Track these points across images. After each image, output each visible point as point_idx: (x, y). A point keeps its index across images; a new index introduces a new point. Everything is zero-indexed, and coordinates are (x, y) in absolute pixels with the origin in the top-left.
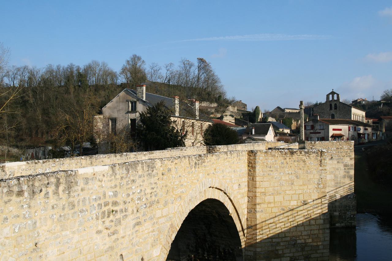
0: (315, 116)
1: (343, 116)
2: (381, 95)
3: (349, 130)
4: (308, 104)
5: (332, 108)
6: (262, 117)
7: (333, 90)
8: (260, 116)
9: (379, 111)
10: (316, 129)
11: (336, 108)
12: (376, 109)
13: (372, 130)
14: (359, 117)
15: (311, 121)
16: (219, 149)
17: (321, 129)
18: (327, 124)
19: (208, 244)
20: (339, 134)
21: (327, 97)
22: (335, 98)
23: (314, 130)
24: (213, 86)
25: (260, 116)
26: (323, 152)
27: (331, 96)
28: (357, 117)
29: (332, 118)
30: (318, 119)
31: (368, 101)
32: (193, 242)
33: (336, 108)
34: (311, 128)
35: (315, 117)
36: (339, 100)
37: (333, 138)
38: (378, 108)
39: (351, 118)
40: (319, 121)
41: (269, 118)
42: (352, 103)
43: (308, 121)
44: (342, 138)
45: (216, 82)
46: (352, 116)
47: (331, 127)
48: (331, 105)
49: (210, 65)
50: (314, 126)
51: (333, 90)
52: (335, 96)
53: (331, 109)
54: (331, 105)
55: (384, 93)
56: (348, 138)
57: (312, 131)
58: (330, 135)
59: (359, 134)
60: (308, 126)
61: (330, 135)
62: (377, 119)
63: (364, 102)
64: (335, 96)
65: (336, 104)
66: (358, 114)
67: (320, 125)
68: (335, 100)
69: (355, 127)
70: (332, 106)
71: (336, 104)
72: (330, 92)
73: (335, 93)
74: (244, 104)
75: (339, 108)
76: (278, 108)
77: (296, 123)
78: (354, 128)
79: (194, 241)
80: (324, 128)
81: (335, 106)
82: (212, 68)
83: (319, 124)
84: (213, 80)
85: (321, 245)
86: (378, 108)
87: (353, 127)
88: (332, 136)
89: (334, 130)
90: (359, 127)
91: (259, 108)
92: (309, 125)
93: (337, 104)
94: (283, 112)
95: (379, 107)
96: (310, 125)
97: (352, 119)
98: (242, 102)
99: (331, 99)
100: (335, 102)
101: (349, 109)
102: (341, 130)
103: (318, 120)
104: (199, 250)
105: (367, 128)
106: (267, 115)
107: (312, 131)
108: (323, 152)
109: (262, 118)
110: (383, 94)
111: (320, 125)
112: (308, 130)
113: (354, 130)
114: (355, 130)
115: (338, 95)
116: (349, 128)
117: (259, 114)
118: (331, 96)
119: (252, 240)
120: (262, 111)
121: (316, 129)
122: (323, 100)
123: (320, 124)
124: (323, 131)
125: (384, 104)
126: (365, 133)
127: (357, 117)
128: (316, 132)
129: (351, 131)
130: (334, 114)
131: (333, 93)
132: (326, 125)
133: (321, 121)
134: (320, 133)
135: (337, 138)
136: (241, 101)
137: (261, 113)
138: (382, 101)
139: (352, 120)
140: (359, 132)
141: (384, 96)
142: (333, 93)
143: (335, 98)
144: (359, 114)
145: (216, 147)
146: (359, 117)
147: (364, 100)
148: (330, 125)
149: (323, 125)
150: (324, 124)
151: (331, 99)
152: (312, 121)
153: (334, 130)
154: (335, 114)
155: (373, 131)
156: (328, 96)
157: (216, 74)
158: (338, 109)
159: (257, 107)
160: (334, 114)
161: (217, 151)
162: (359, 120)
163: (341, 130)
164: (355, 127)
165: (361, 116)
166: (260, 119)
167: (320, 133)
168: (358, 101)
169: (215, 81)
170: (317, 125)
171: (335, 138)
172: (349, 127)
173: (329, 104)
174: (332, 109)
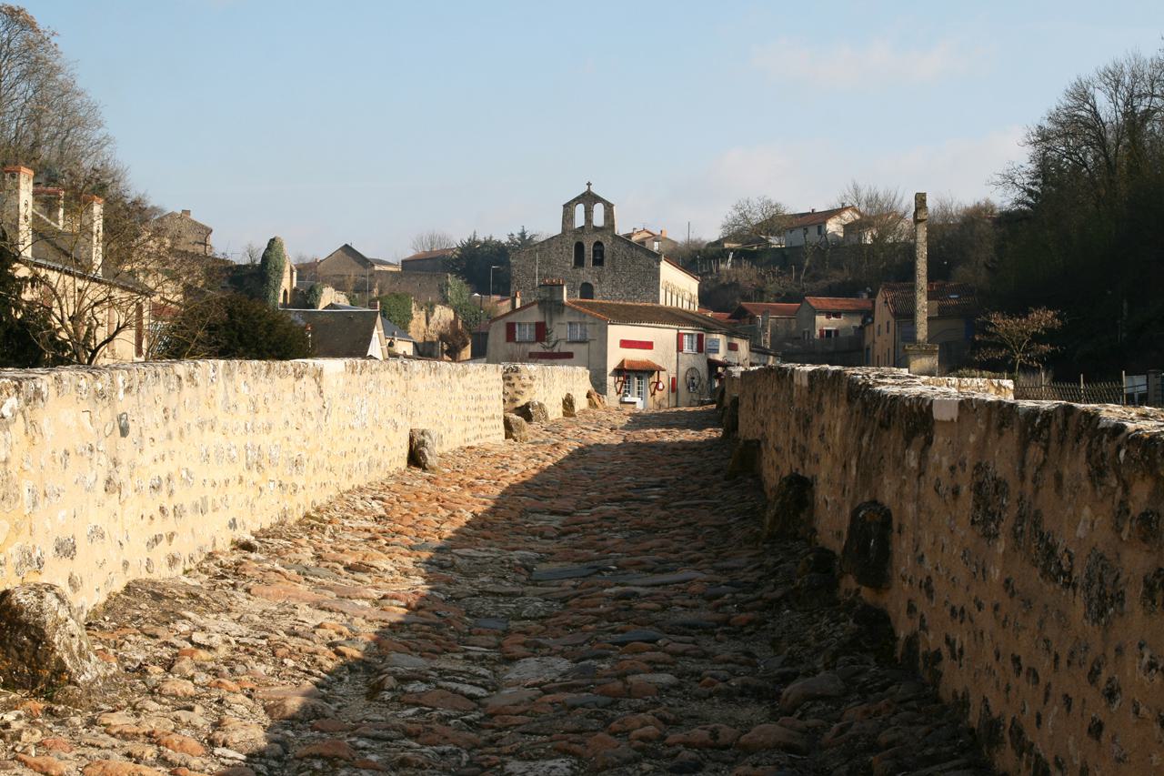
0: (554, 285)
1: (628, 293)
2: (725, 220)
3: (680, 348)
4: (432, 243)
5: (586, 258)
6: (295, 285)
7: (589, 184)
8: (287, 283)
9: (724, 280)
10: (554, 339)
11: (598, 261)
12: (711, 272)
13: (751, 350)
14: (680, 300)
16: (530, 378)
17: (574, 338)
18: (599, 318)
20: (643, 363)
22: (598, 220)
23: (546, 344)
24: (69, 139)
25: (287, 283)
26: (1004, 388)
28: (674, 297)
29: (581, 297)
30: (565, 299)
31: (675, 243)
33: (598, 261)
34: (534, 333)
35: (551, 290)
36: (613, 226)
37: (621, 379)
38: (717, 271)
39: (658, 302)
40: (570, 307)
41: (325, 290)
44: (651, 380)
45: (81, 123)
46: (662, 292)
47: (616, 332)
48: (579, 247)
49: (54, 40)
50: (548, 326)
51: (589, 184)
52: (599, 210)
53: (579, 262)
54: (579, 247)
55: (736, 214)
56: (673, 379)
57: (537, 348)
58: (612, 364)
59: (713, 365)
60: (519, 324)
61: (612, 364)
62: (729, 314)
63: (656, 244)
64: (599, 210)
65: (598, 244)
66: (679, 286)
67: (570, 323)
68: (597, 229)
69: (700, 337)
70: (586, 250)
71: (598, 244)
73: (597, 199)
74: (203, 227)
75: (614, 259)
76: (347, 249)
77: (424, 317)
78: (695, 339)
80: (589, 337)
81: (594, 251)
82: (63, 56)
83: (566, 318)
84: (65, 111)
86: (717, 271)
87: (692, 334)
88: (619, 371)
89: (626, 344)
90: (715, 336)
91: (281, 244)
92: (525, 324)
93: (605, 245)
94: (366, 267)
95: (722, 266)
96: (530, 324)
97: (662, 302)
98: (193, 216)
99: (579, 220)
100: (599, 237)
101: (650, 266)
102: (648, 345)
103: (563, 305)
105: (736, 341)
106: (311, 276)
107: (537, 348)
108: (1003, 390)
109: (295, 291)
110: (729, 216)
111: (570, 323)
112: (520, 342)
113: (695, 346)
114: (700, 349)
115: (609, 207)
116: (680, 337)
117: (280, 272)
119: (571, 739)
120: (292, 254)
121: (554, 339)
122: (547, 225)
123: (571, 320)
124: (583, 348)
125: (740, 255)
126: (730, 359)
127: (674, 297)
128: (556, 350)
129: (686, 349)
130: (590, 285)
131: (589, 199)
132: (594, 324)
133: (574, 309)
135: (636, 379)
136: (187, 212)
137: (287, 269)
138: (726, 245)
139: (662, 307)
140: (712, 356)
141: (733, 226)
142: (589, 199)
143: (598, 220)
144: (670, 282)
145: (517, 370)
146: (680, 300)
147: (655, 238)
149: (581, 324)
150: (588, 319)
151: (579, 220)
152: (539, 307)
153: (626, 344)
154: (594, 285)
155: (755, 354)
156: (568, 208)
157: (80, 84)
158: (606, 263)
159: (273, 240)
160: (590, 282)
161: (523, 386)
162: (680, 306)
163: (648, 345)
164: (700, 337)
165: (687, 296)
166: (285, 292)
168: (634, 239)
169: (74, 120)
170: (559, 324)
171: (628, 377)
172: (678, 334)
173: (572, 242)
174: (586, 262)
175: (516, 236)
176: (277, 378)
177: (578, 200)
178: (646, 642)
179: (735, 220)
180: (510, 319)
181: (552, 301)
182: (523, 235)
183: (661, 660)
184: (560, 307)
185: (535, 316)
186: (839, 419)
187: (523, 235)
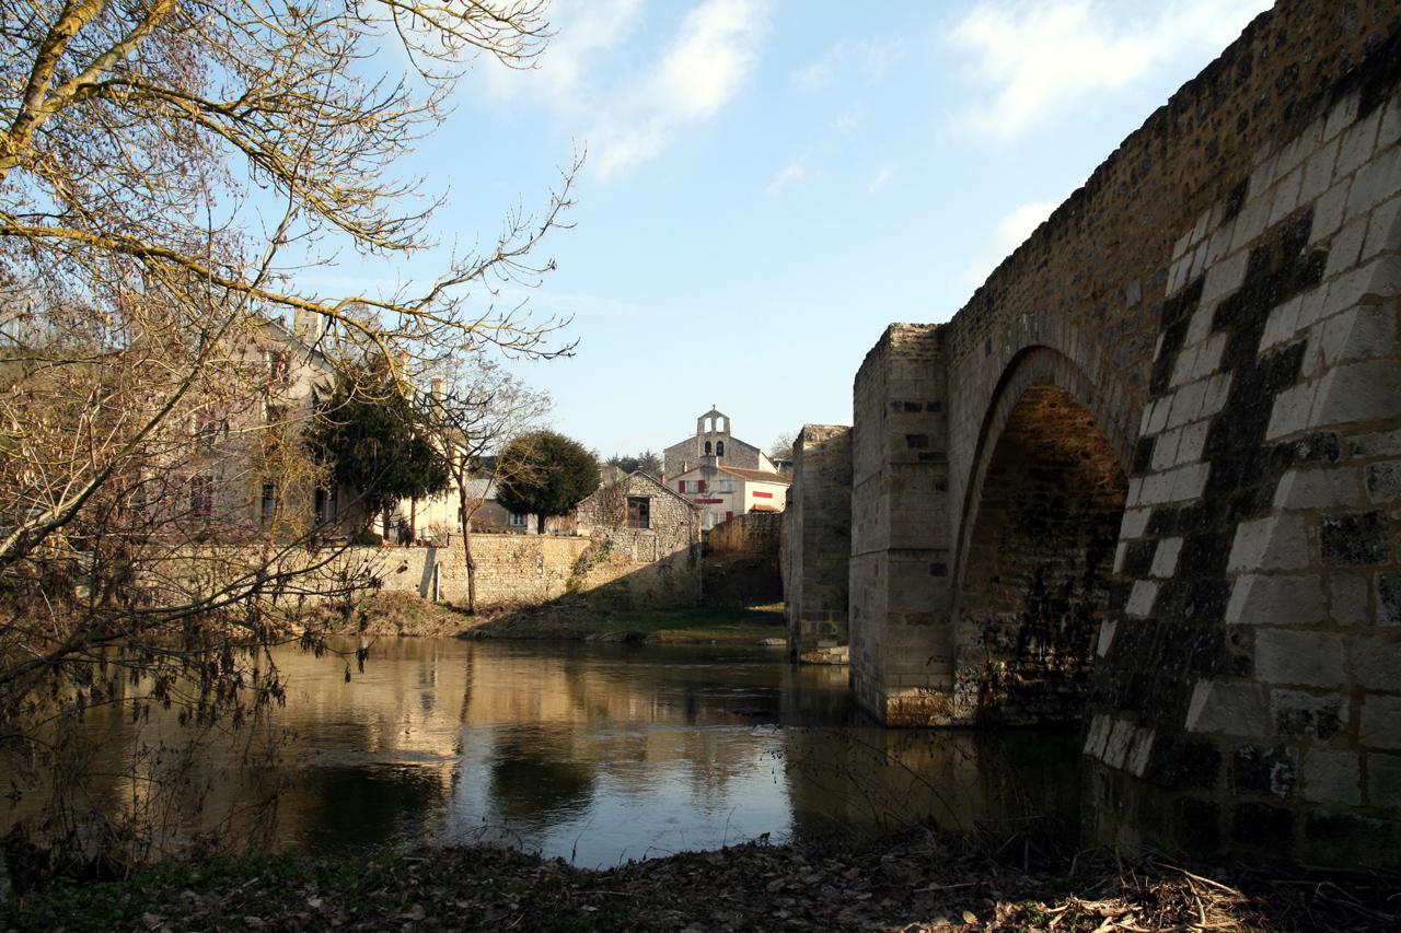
15: (698, 471)
17: (724, 490)
19: (1068, 618)
21: (699, 423)
22: (720, 427)
27: (708, 422)
32: (1015, 618)
33: (720, 453)
42: (31, 842)
43: (689, 472)
48: (708, 445)
54: (708, 445)
55: (780, 441)
57: (700, 496)
72: (707, 412)
73: (719, 415)
79: (1022, 612)
83: (718, 477)
85: (1265, 625)
89: (756, 494)
100: (719, 438)
102: (769, 496)
104: (1029, 644)
107: (700, 496)
111: (721, 481)
115: (727, 420)
118: (708, 422)
123: (722, 478)
124: (730, 496)
131: (714, 415)
134: (720, 501)
142: (714, 415)
148: (850, 423)
150: (733, 478)
151: (708, 428)
153: (756, 494)
156: (701, 420)
163: (769, 496)
167: (720, 501)
175: (644, 454)
176: (513, 380)
177: (707, 415)
178: (340, 725)
179: (779, 444)
180: (681, 479)
181: (709, 467)
182: (648, 454)
183: (344, 722)
184: (714, 471)
185: (698, 476)
186: (1268, 377)
187: (648, 454)
